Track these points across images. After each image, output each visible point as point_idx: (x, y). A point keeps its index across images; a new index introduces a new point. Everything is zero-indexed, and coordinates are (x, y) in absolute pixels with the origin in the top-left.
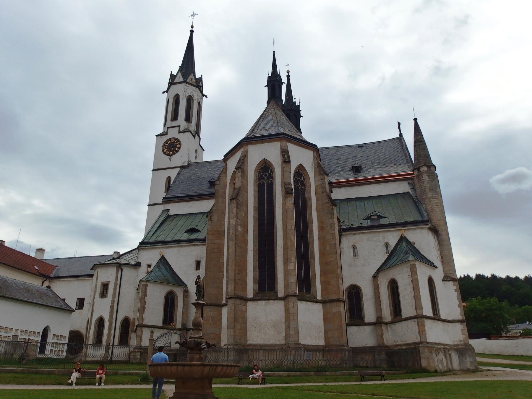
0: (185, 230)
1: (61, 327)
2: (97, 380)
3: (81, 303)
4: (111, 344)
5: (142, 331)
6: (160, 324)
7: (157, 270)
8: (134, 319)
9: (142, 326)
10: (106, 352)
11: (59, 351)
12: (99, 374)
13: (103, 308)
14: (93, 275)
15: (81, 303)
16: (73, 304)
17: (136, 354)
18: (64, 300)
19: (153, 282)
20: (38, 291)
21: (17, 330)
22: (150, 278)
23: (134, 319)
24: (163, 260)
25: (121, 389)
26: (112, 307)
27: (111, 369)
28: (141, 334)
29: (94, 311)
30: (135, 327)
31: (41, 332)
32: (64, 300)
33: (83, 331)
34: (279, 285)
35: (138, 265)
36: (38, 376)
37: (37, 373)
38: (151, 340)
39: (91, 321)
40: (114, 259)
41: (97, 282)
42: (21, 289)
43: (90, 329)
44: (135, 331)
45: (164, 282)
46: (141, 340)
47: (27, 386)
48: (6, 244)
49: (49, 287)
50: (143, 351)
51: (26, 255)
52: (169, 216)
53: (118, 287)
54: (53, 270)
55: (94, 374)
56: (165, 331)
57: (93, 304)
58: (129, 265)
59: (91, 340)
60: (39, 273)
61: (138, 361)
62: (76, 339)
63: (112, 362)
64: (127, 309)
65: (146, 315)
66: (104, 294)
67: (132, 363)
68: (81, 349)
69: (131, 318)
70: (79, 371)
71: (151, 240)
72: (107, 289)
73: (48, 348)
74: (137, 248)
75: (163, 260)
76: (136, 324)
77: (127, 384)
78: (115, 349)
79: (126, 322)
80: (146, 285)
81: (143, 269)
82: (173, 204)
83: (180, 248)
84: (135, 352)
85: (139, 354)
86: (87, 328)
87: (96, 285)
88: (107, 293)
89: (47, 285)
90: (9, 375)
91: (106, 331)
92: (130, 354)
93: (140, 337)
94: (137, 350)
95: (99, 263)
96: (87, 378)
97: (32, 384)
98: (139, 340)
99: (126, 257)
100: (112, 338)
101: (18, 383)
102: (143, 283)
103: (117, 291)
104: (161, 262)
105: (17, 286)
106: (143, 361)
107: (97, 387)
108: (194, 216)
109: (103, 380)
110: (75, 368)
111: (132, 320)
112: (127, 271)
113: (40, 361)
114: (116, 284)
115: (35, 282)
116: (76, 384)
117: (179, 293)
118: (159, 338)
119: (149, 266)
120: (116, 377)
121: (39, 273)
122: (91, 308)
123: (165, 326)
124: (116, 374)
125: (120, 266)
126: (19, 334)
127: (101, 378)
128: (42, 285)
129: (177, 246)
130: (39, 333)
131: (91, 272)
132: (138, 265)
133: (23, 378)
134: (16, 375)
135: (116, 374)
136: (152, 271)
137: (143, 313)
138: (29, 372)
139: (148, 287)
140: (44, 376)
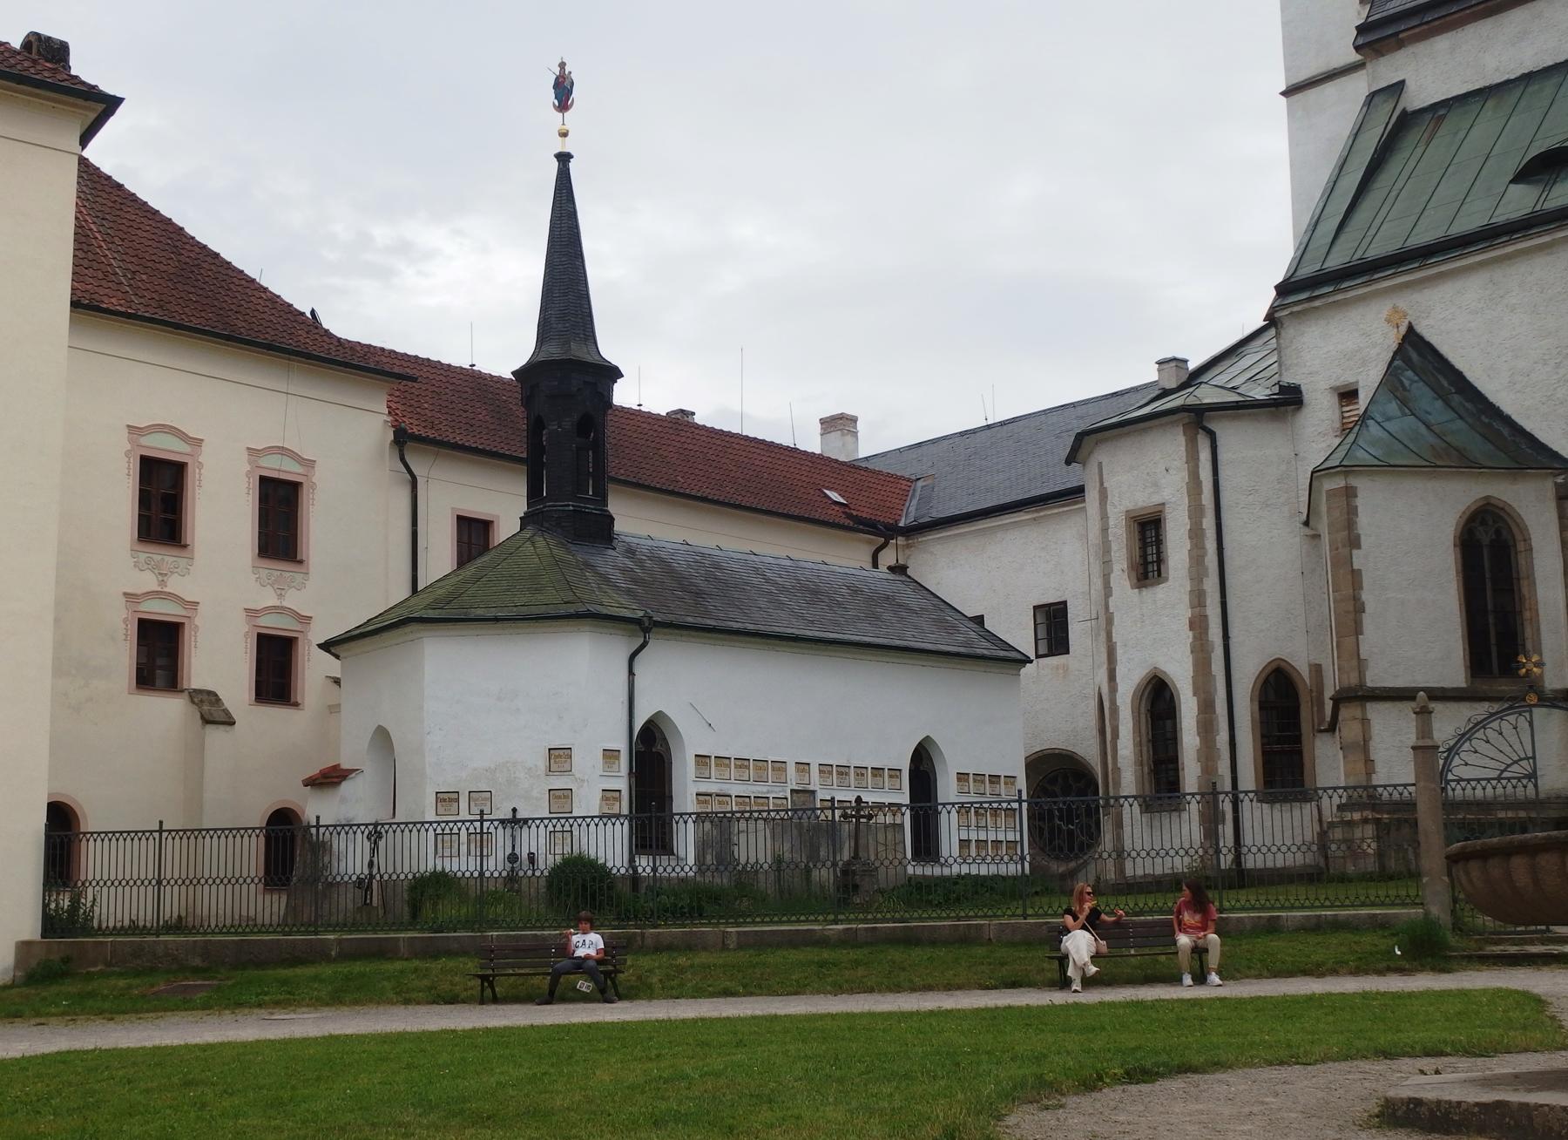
0: (1513, 164)
1: (989, 736)
2: (1184, 959)
3: (1053, 624)
4: (1228, 787)
5: (1365, 722)
6: (1453, 670)
7: (1393, 408)
8: (1317, 669)
9: (1359, 695)
10: (1211, 833)
11: (997, 843)
12: (1184, 929)
13: (1153, 635)
14: (1077, 493)
15: (1053, 624)
16: (1022, 637)
17: (1358, 833)
18: (979, 620)
19: (1383, 468)
20: (855, 591)
21: (803, 766)
22: (1360, 454)
23: (1317, 669)
24: (1415, 352)
25: (1310, 999)
26: (1198, 624)
27: (1241, 909)
28: (1366, 740)
29: (1119, 651)
30: (1329, 705)
31: (905, 765)
32: (979, 620)
33: (1088, 750)
34: (1474, 974)
35: (1289, 399)
36: (917, 954)
37: (909, 940)
38: (1424, 751)
39: (1113, 702)
40: (1165, 393)
41: (1104, 517)
42: (783, 589)
43: (1116, 735)
44: (1332, 728)
45: (1446, 460)
46: (1369, 763)
47: (877, 997)
48: (699, 419)
49: (899, 569)
50: (1392, 817)
51: (779, 447)
52: (1406, 122)
53: (1208, 523)
54: (904, 495)
55: (1166, 934)
56: (1481, 710)
57: (1110, 621)
58: (1243, 408)
59: (1129, 780)
60: (850, 516)
61: (1371, 865)
62: (1062, 792)
63: (1241, 878)
64: (1276, 622)
65: (1371, 641)
66: (1148, 566)
67: (1343, 879)
68: (1094, 834)
69: (1301, 665)
70: (1092, 922)
71: (1335, 261)
72: (1159, 542)
73: (951, 831)
74: (1272, 320)
75: (1415, 352)
76: (1329, 693)
77: (1334, 972)
78: (1246, 806)
79: (1280, 693)
80: (1350, 493)
81: (1320, 414)
82: (1421, 48)
83: (1498, 273)
84: (1350, 824)
85: (1369, 830)
86: (1102, 732)
87: (1105, 530)
88: (1160, 560)
89: (893, 562)
90: (794, 955)
91: (1189, 739)
92: (1323, 835)
93: (1362, 749)
94: (1357, 816)
95: (1096, 431)
96: (1135, 950)
97: (896, 988)
98: (1360, 766)
99: (1222, 376)
100: (1224, 767)
101: (838, 989)
102: (1329, 484)
103: (1211, 546)
104: (1409, 363)
105: (768, 580)
106: (1392, 865)
107: (1187, 990)
108: (1549, 87)
109: (1214, 959)
110: (1069, 911)
111: (1305, 672)
112: (1236, 441)
113: (922, 893)
114: (1196, 511)
115: (844, 558)
116: (1089, 982)
117: (1534, 507)
118: (1465, 737)
119: (1348, 395)
120: (1276, 944)
121: (850, 516)
122: (1103, 634)
123: (1484, 687)
124: (1272, 928)
125: (1198, 420)
126: (815, 782)
127: (1199, 951)
128: (875, 565)
129: (1482, 264)
130: (895, 773)
131: (1067, 478)
132: (1289, 399)
133: (856, 963)
134: (826, 954)
135: (1272, 928)
136: (1365, 417)
137: (1358, 630)
138: (877, 940)
139: (1360, 502)
140: (941, 952)
